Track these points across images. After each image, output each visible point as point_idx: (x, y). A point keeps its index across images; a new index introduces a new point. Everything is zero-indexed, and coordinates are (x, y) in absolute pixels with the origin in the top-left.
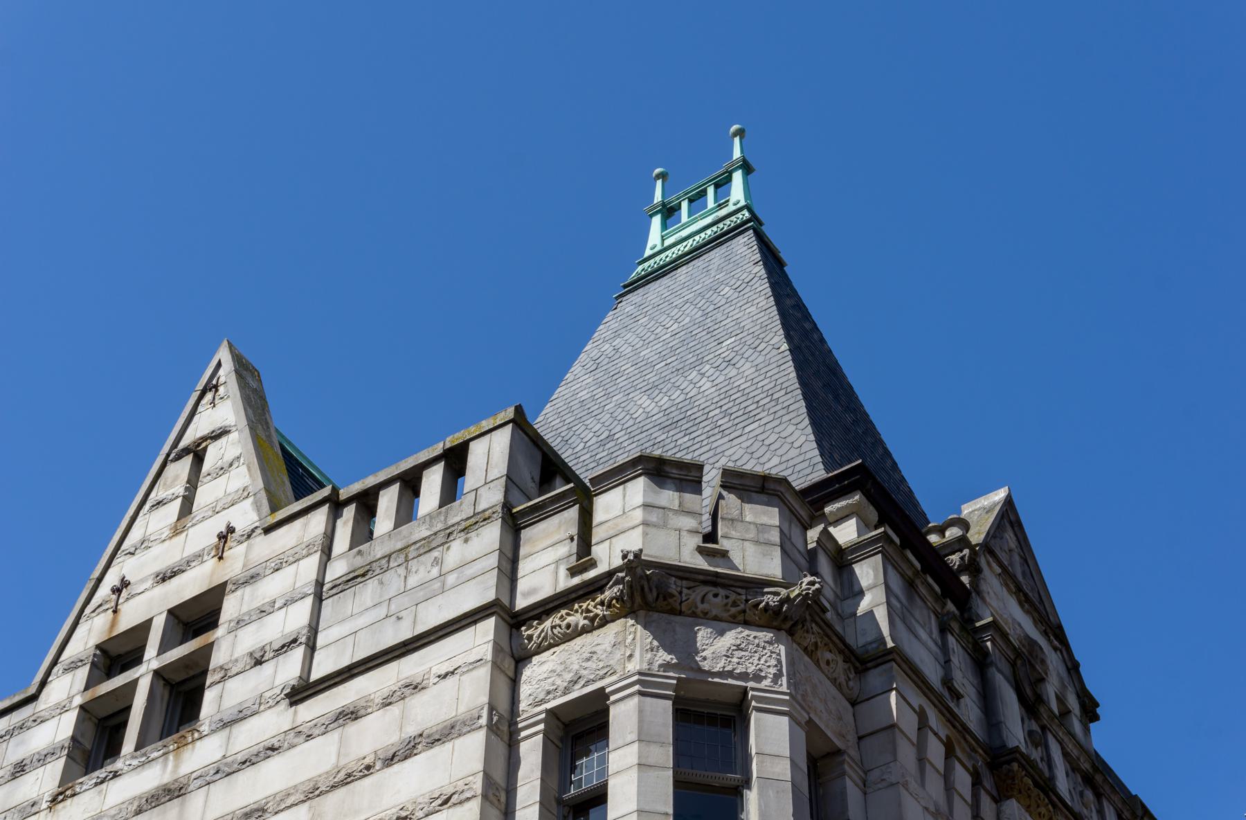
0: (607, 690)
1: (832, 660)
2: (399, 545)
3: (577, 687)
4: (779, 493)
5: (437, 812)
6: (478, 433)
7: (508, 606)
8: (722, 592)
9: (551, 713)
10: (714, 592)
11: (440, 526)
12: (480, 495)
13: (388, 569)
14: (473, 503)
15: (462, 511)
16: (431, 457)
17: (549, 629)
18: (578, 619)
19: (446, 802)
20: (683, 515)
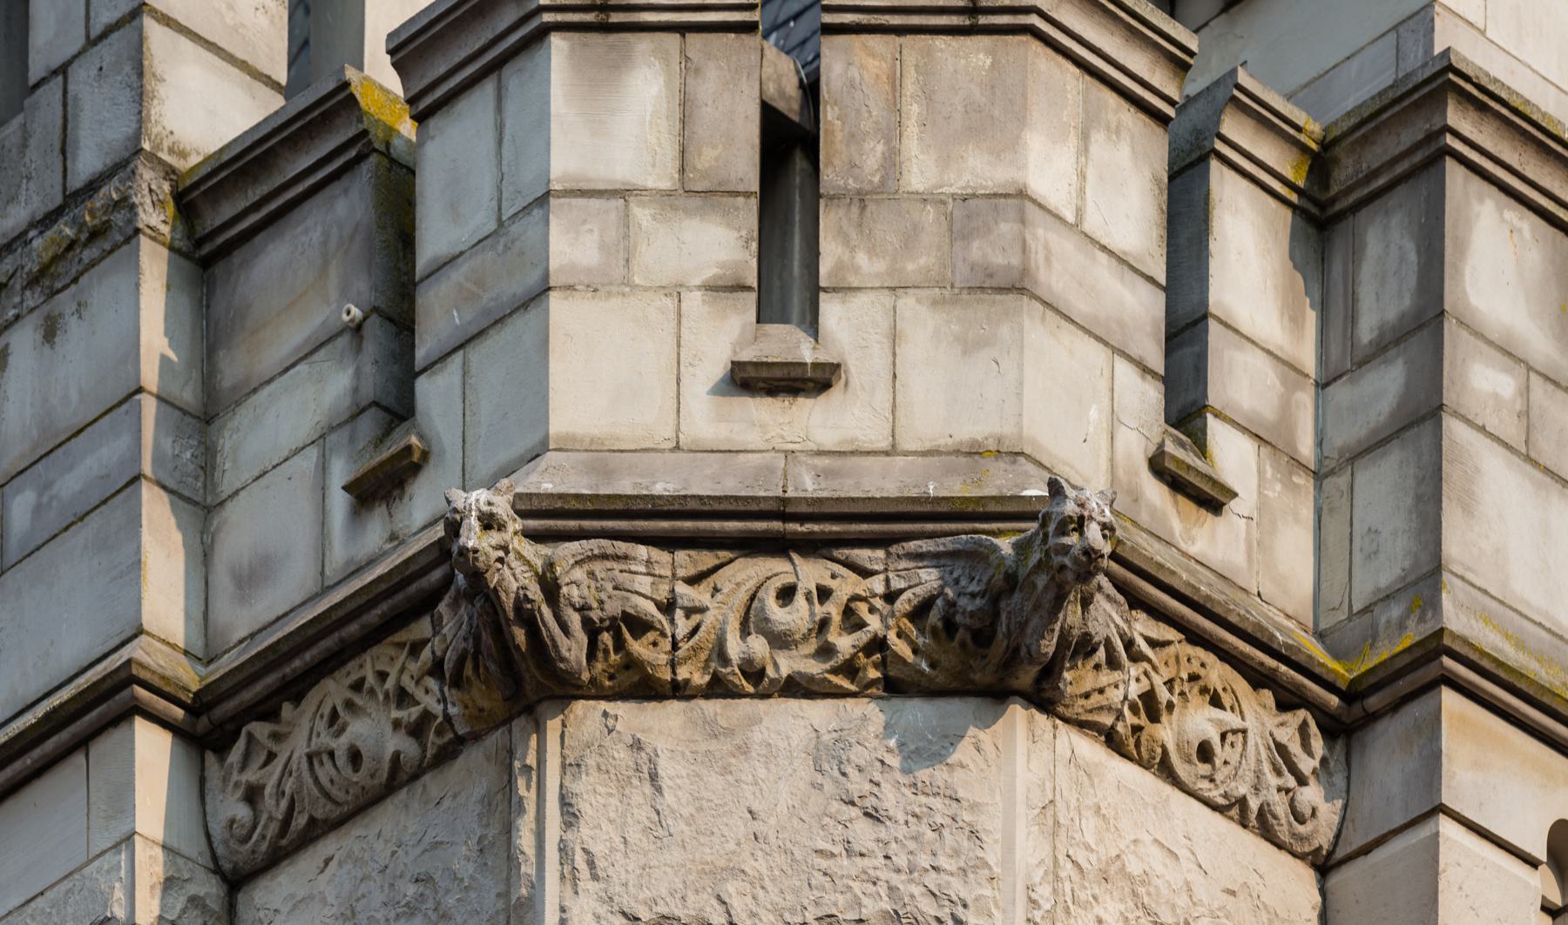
1: (1223, 736)
4: (1034, 20)
7: (417, 280)
8: (810, 572)
10: (777, 583)
12: (76, 98)
14: (58, 146)
15: (29, 178)
17: (305, 765)
20: (688, 213)
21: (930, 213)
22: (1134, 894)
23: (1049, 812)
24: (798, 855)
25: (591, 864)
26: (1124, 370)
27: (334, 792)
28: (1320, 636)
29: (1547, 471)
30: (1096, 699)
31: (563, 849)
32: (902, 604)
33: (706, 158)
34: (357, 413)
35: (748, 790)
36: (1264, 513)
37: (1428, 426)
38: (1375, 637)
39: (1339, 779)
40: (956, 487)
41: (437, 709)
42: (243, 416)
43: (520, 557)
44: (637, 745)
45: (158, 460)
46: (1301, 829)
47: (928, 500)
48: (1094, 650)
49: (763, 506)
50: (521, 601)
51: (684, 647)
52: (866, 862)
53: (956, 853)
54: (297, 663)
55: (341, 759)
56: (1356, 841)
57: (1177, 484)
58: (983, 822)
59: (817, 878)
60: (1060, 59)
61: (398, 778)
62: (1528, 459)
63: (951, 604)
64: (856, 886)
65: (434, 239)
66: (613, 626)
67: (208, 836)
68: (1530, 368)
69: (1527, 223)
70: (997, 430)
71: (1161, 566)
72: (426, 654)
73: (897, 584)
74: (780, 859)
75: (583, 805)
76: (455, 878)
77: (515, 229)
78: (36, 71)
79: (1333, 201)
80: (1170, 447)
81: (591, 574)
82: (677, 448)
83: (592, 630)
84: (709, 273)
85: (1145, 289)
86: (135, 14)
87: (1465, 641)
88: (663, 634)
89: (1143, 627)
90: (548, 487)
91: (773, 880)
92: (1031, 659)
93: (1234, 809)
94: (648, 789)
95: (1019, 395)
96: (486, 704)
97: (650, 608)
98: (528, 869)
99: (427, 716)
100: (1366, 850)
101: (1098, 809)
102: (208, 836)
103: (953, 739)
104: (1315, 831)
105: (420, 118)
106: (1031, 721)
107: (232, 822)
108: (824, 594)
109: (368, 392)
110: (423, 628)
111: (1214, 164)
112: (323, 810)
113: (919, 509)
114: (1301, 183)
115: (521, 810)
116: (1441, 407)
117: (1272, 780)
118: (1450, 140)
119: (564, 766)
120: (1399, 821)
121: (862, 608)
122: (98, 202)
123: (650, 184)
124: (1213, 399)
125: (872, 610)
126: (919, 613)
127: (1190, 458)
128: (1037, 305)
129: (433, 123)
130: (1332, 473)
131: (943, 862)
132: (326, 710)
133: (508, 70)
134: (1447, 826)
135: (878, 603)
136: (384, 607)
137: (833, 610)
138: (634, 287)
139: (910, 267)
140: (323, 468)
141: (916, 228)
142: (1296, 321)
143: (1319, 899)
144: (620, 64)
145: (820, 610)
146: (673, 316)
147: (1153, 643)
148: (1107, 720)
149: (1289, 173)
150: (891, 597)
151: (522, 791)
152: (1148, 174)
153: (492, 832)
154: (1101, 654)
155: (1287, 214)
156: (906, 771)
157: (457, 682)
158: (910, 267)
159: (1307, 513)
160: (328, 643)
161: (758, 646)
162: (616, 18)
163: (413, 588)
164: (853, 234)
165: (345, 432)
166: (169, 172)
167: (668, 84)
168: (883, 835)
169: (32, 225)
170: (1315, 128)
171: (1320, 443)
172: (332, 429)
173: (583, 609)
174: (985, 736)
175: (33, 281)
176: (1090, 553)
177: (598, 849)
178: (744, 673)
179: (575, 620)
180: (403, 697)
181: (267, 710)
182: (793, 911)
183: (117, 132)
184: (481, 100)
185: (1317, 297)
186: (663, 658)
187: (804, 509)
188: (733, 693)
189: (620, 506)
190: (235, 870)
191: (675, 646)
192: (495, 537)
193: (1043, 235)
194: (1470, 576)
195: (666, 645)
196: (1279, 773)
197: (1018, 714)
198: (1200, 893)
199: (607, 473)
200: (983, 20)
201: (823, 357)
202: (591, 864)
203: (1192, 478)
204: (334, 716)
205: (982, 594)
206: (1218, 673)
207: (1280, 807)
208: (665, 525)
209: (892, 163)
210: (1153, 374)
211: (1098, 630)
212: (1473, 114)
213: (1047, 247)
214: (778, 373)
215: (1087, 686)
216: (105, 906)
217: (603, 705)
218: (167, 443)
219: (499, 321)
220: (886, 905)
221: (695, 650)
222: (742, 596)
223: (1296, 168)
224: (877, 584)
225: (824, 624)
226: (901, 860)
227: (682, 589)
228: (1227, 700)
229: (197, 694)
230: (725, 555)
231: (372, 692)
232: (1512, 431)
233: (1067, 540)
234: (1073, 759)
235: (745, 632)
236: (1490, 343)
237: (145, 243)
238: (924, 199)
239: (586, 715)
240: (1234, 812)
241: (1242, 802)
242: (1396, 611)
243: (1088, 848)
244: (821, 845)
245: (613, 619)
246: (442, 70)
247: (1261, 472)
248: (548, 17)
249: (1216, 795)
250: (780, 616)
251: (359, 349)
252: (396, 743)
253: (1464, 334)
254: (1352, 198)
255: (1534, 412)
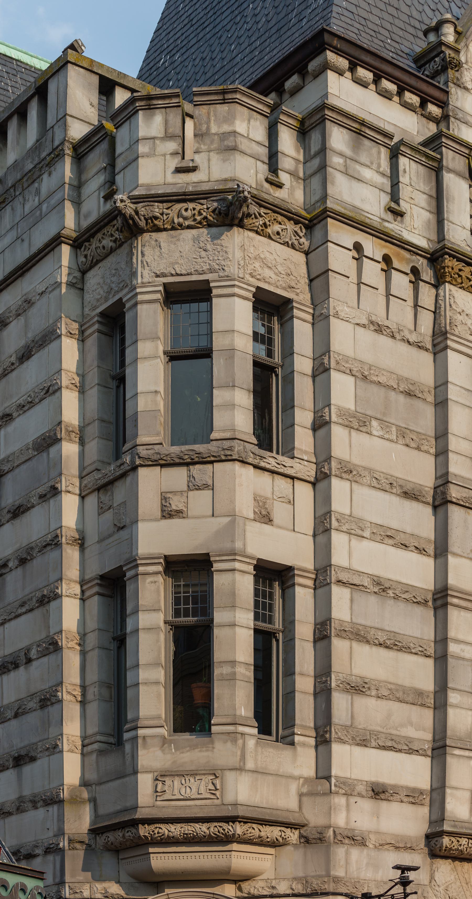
0: (124, 300)
1: (282, 230)
2: (19, 177)
3: (111, 296)
5: (44, 399)
6: (51, 74)
8: (191, 205)
9: (102, 314)
10: (184, 208)
11: (37, 161)
13: (15, 196)
16: (29, 95)
18: (107, 242)
19: (47, 391)
20: (167, 141)
21: (216, 137)
22: (263, 261)
23: (243, 247)
24: (190, 259)
25: (147, 264)
26: (259, 163)
27: (101, 254)
28: (305, 210)
29: (351, 176)
30: (252, 225)
31: (142, 261)
32: (210, 210)
33: (170, 130)
34: (105, 183)
35: (179, 247)
36: (292, 189)
37: (324, 169)
38: (315, 209)
39: (309, 237)
40: (221, 187)
41: (118, 237)
42: (85, 186)
43: (130, 207)
44: (156, 241)
45: (68, 196)
46: (301, 247)
47: (214, 190)
48: (251, 215)
49: (180, 194)
50: (130, 215)
51: (166, 221)
52: (204, 259)
53: (222, 256)
54: (92, 231)
55: (101, 248)
56: (313, 248)
57: (271, 183)
58: (228, 250)
59: (194, 263)
60: (243, 107)
61: (112, 251)
62: (346, 174)
63: (220, 209)
64: (202, 264)
65: (119, 149)
66: (151, 218)
67: (78, 265)
68: (346, 157)
69: (345, 131)
70: (230, 176)
71: (265, 199)
72: (116, 227)
73: (209, 206)
74: (186, 260)
75: (146, 253)
76: (122, 269)
77: (133, 147)
78: (48, 128)
79: (306, 129)
80: (269, 177)
81: (146, 209)
82: (165, 184)
83: (146, 220)
84: (171, 151)
85: (263, 148)
86: (65, 116)
87: (332, 209)
88: (161, 219)
89: (262, 211)
90: (137, 193)
91: (185, 264)
92: (237, 218)
93: (286, 244)
94: (159, 249)
95: (235, 169)
96: (127, 235)
97: (159, 215)
98: (135, 266)
99: (116, 238)
100: (315, 250)
101: (254, 246)
102: (78, 265)
103: (222, 234)
104: (304, 247)
105: (116, 128)
106: (238, 230)
107: (82, 262)
108: (194, 209)
109: (107, 179)
110: (115, 222)
111: (279, 124)
112: (99, 258)
113: (212, 191)
114: (298, 126)
115: (134, 255)
116: (326, 165)
117: (294, 238)
118: (326, 116)
119: (142, 246)
120: (320, 244)
121: (202, 211)
122: (58, 150)
123: (159, 136)
124: (279, 167)
125: (204, 211)
126: (214, 211)
127: (276, 179)
128: (239, 152)
129: (118, 129)
130: (307, 179)
131: (220, 258)
132: (98, 239)
133: (131, 118)
134: (330, 244)
135: (205, 210)
136: (108, 219)
137: (196, 212)
138: (156, 155)
139: (212, 147)
140: (99, 194)
141: (213, 140)
142: (298, 152)
143: (306, 260)
144: (153, 115)
145: (193, 212)
146: (164, 160)
147: (265, 213)
148: (256, 229)
149: (295, 125)
150: (208, 209)
151: (134, 251)
152: (264, 126)
153: (128, 259)
154: (253, 216)
155: (296, 132)
156: (212, 241)
157: (121, 231)
158: (212, 147)
159: (302, 187)
160: (98, 226)
161: (181, 220)
162: (152, 107)
163: (113, 215)
164: (200, 142)
165: (103, 187)
166: (72, 143)
167: (163, 118)
168: (207, 254)
169: (47, 155)
170: (301, 116)
171: (304, 174)
172: (101, 187)
173: (144, 216)
174: (228, 234)
175: (47, 166)
176: (246, 198)
177: (149, 261)
178: (179, 225)
179: (142, 218)
180: (112, 235)
181: (88, 240)
182: (189, 270)
183: (61, 137)
184: (127, 124)
185: (303, 147)
186: (161, 224)
187: (189, 193)
188: (177, 229)
189: (151, 196)
190: (83, 271)
191: (164, 221)
192: (123, 204)
193: (239, 139)
194: (334, 197)
195: (162, 221)
196: (295, 236)
197: (235, 229)
198: (278, 260)
199: (150, 190)
200: (226, 101)
201: (194, 165)
202: (147, 264)
203: (274, 182)
204: (100, 240)
205: (226, 207)
206: (280, 218)
207: (296, 243)
208: (161, 199)
209: (208, 128)
210: (266, 163)
211: (251, 211)
212: (331, 112)
213: (241, 141)
214: (185, 169)
215: (251, 222)
216: (56, 279)
217: (150, 234)
218: (71, 193)
219: (130, 164)
220: (208, 267)
221: (168, 222)
222: (177, 211)
223: (297, 124)
224: (205, 206)
225: (194, 215)
226: (211, 258)
227: (165, 210)
228: (283, 223)
229: (75, 238)
230: (173, 203)
231: (106, 235)
232: (343, 169)
233: (241, 195)
234: (248, 237)
235: (178, 217)
236: (337, 153)
237: (66, 156)
238: (215, 134)
239: (146, 236)
240: (286, 244)
241: (287, 242)
242: (319, 204)
243: (251, 253)
244: (195, 257)
245: (151, 217)
246: (120, 119)
247: (291, 180)
248: (138, 108)
249: (281, 241)
250: (185, 214)
251: (105, 172)
252: (111, 244)
253: (331, 152)
254: (309, 128)
255: (348, 165)
